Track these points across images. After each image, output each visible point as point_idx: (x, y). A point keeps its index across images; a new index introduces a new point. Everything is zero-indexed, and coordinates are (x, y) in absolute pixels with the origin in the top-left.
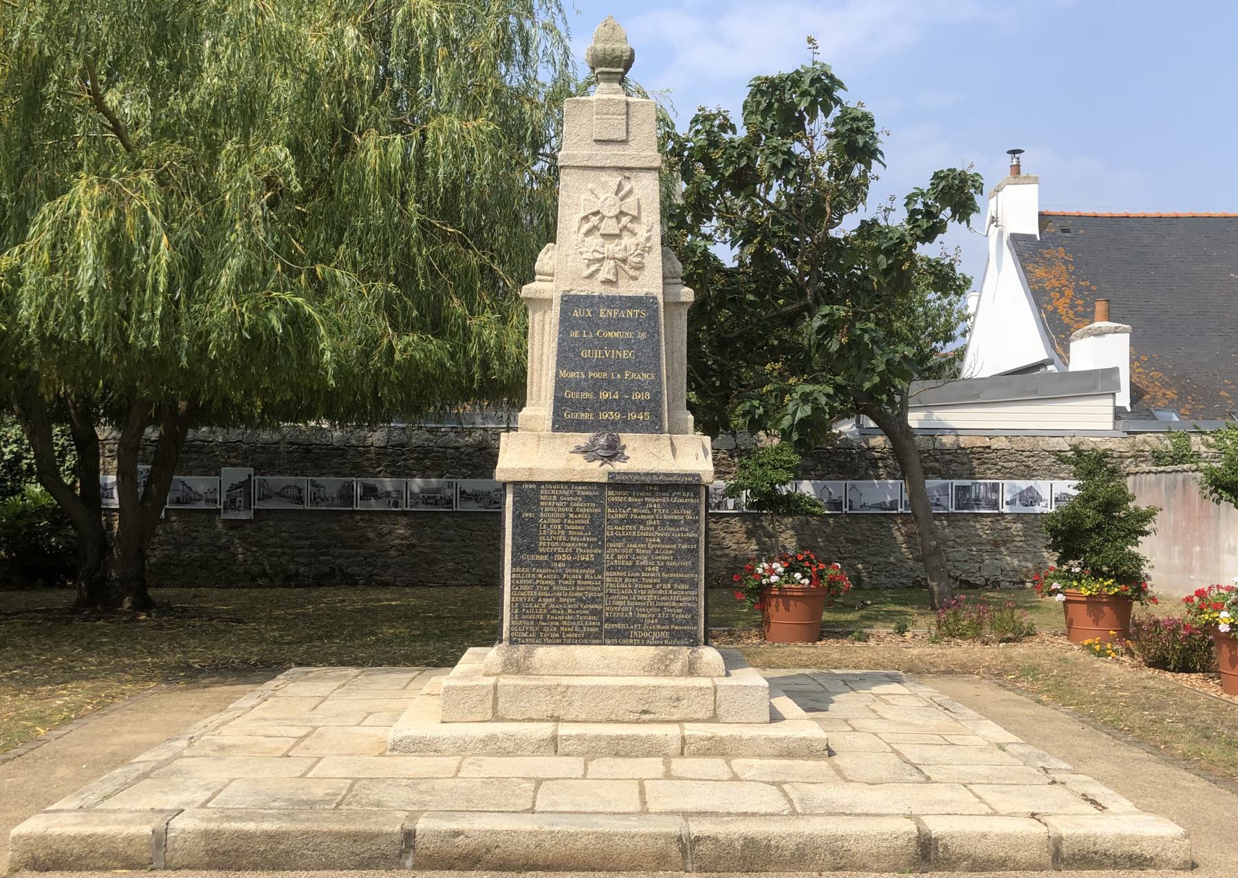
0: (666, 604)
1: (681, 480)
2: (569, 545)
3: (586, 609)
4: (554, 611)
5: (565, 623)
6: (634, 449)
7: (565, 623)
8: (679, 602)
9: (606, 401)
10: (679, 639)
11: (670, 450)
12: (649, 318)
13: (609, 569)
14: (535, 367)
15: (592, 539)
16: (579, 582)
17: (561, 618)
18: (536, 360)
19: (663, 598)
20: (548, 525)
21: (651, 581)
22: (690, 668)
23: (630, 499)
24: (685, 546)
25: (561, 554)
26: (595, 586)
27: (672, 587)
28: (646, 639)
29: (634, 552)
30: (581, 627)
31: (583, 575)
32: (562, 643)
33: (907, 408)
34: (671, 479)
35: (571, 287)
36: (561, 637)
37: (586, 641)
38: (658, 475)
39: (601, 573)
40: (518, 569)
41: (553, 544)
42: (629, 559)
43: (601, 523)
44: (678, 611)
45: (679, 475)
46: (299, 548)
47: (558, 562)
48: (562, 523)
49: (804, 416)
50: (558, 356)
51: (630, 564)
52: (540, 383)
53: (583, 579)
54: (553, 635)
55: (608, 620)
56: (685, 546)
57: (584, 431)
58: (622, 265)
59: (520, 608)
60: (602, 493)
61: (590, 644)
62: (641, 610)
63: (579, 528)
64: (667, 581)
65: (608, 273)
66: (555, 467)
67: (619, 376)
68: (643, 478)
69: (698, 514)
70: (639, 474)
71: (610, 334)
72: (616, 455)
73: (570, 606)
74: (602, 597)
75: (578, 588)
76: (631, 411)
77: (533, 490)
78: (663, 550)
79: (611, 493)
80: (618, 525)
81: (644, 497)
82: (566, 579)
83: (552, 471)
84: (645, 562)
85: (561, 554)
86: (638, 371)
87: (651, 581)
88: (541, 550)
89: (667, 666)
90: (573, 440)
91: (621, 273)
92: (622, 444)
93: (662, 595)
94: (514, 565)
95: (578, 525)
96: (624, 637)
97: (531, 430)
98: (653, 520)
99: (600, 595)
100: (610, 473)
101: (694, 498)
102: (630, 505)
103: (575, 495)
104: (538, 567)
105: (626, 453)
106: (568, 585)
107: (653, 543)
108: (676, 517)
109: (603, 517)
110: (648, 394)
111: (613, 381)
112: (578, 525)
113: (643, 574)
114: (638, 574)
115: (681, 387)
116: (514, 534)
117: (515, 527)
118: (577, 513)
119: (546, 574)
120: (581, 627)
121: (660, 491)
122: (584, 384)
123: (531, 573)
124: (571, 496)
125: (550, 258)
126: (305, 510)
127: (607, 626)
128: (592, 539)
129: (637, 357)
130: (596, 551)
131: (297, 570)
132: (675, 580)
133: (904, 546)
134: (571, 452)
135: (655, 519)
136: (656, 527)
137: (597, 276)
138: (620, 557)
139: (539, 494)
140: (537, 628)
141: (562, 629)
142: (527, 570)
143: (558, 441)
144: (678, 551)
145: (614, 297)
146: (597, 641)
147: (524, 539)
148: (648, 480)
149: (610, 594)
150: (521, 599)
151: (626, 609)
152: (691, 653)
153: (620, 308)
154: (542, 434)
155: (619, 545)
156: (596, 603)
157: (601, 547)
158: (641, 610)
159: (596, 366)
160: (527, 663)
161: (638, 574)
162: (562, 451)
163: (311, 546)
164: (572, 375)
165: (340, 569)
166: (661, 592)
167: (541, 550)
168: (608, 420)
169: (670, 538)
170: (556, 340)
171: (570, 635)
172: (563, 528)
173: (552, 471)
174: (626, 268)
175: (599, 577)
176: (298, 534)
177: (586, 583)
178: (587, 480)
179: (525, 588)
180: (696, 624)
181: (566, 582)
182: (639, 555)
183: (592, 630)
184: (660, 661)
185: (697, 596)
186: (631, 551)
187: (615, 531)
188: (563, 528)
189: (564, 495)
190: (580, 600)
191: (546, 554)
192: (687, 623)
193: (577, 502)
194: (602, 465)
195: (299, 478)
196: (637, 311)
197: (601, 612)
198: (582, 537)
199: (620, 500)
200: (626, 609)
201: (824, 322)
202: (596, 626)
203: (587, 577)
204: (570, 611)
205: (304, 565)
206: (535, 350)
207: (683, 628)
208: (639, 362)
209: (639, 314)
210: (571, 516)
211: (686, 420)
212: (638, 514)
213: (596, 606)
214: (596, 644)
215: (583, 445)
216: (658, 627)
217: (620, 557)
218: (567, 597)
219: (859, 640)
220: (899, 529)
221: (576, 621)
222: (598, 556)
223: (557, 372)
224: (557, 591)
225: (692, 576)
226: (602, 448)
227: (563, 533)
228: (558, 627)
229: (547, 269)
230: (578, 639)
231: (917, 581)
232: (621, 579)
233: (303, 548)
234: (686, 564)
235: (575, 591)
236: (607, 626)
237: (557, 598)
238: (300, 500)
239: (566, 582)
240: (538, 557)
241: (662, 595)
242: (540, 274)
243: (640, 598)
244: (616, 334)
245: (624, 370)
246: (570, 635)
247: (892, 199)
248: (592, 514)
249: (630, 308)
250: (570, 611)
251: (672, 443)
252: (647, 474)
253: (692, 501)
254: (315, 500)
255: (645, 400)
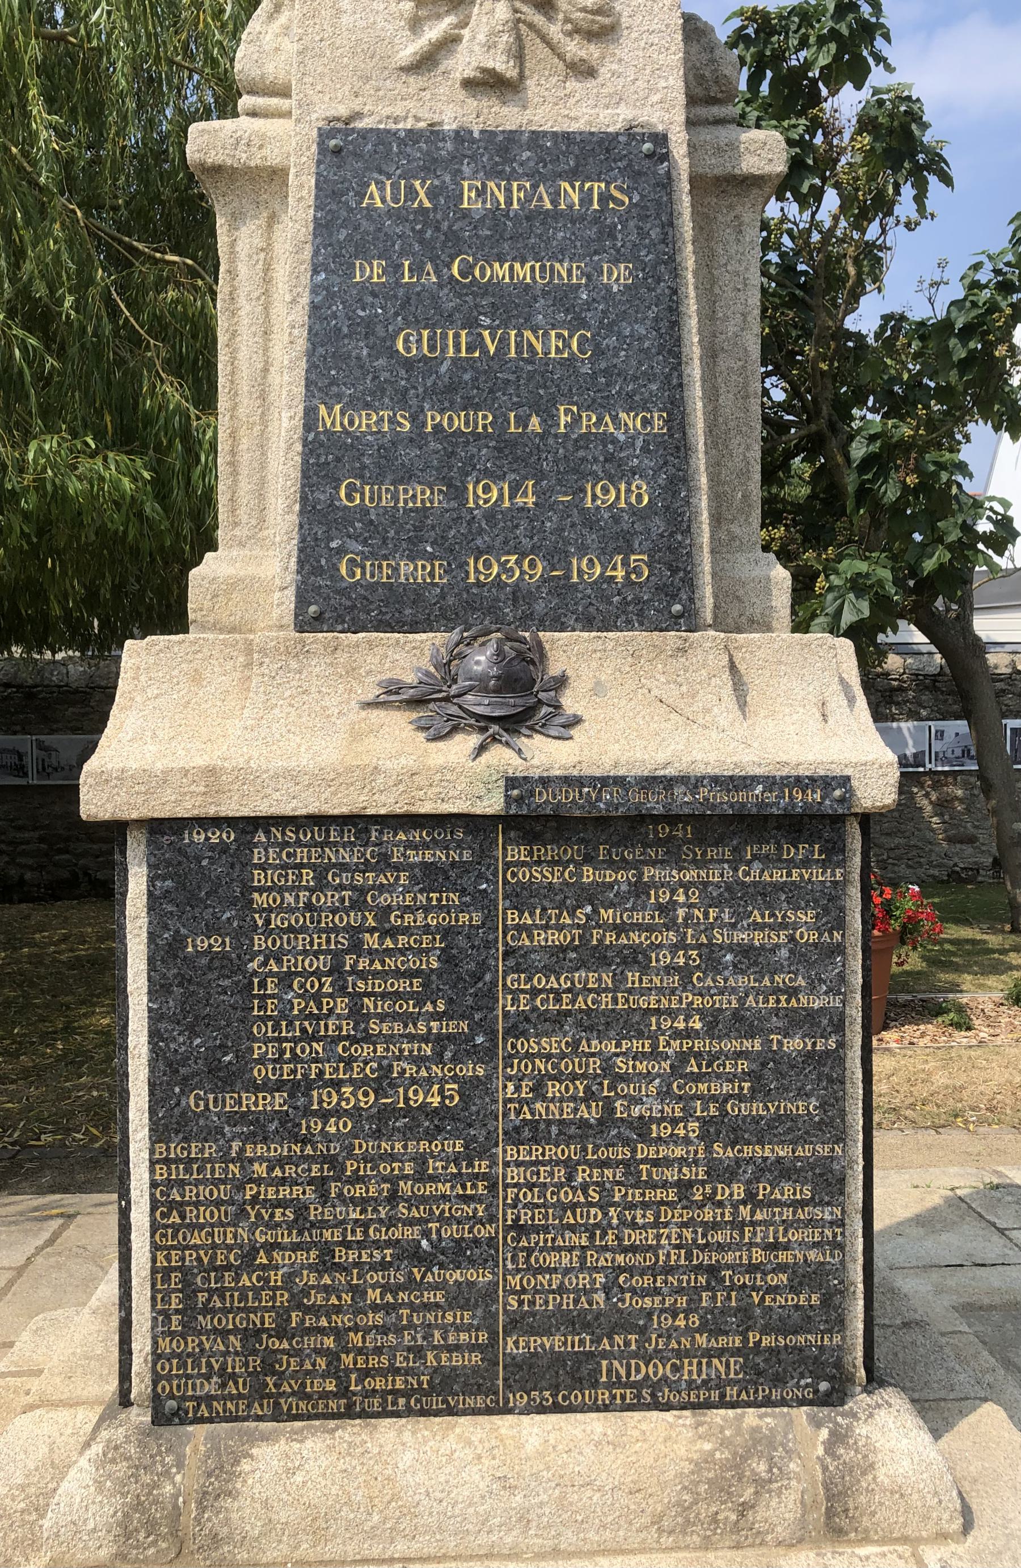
0: (730, 1257)
1: (778, 802)
2: (366, 1050)
3: (435, 1287)
4: (317, 1299)
5: (356, 1339)
6: (598, 689)
7: (356, 1339)
8: (775, 1246)
9: (491, 515)
10: (778, 1381)
11: (728, 690)
12: (640, 212)
13: (514, 1136)
14: (242, 411)
15: (450, 1027)
16: (405, 1188)
17: (342, 1320)
18: (244, 387)
19: (719, 1237)
20: (285, 980)
21: (671, 1175)
22: (830, 1514)
23: (589, 875)
24: (794, 1044)
25: (337, 1084)
26: (466, 1199)
27: (751, 1197)
28: (655, 1387)
29: (607, 1068)
30: (418, 1352)
31: (421, 1160)
32: (349, 1413)
33: (972, 609)
34: (741, 796)
35: (356, 105)
36: (344, 1391)
37: (436, 1402)
38: (692, 782)
39: (485, 1152)
40: (176, 1150)
41: (303, 1049)
42: (590, 1096)
43: (483, 966)
44: (773, 1280)
45: (770, 782)
46: (22, 843)
47: (325, 1116)
48: (336, 970)
49: (855, 619)
50: (310, 354)
51: (591, 1113)
52: (263, 466)
53: (421, 1176)
54: (315, 1386)
55: (516, 1324)
56: (794, 1044)
57: (414, 628)
58: (539, 19)
59: (189, 1291)
60: (484, 854)
61: (451, 1412)
62: (637, 1282)
63: (401, 985)
64: (728, 1173)
65: (490, 46)
66: (304, 760)
67: (535, 423)
68: (636, 797)
69: (840, 924)
70: (620, 781)
71: (501, 271)
72: (529, 712)
73: (377, 1277)
74: (492, 1241)
75: (402, 1209)
76: (583, 550)
77: (223, 848)
78: (713, 1057)
79: (517, 853)
80: (548, 971)
81: (637, 865)
82: (357, 1179)
83: (292, 776)
84: (651, 1107)
85: (337, 1084)
86: (602, 404)
87: (671, 1175)
88: (258, 1073)
89: (744, 1509)
90: (372, 660)
91: (536, 49)
92: (554, 669)
93: (715, 1226)
94: (159, 1133)
95: (398, 974)
96: (578, 1382)
97: (233, 630)
98: (674, 948)
99: (484, 1232)
100: (511, 782)
101: (824, 864)
102: (592, 895)
103: (384, 862)
104: (249, 1138)
105: (571, 702)
106: (363, 1203)
107: (677, 1034)
108: (758, 938)
109: (490, 944)
110: (641, 486)
111: (513, 443)
112: (398, 974)
113: (643, 1151)
114: (622, 1153)
115: (744, 474)
116: (155, 1017)
117: (157, 989)
118: (393, 932)
119: (281, 1162)
120: (418, 1352)
121: (700, 840)
122: (408, 454)
123: (226, 1159)
124: (366, 867)
125: (286, 30)
126: (29, 787)
127: (512, 1346)
128: (450, 1027)
129: (599, 352)
130: (468, 1070)
131: (22, 877)
132: (763, 1169)
133: (934, 820)
134: (368, 705)
135: (681, 945)
136: (685, 973)
137: (446, 64)
138: (553, 1089)
139: (247, 864)
140: (255, 1362)
141: (347, 1360)
142: (210, 1150)
143: (317, 666)
144: (769, 1058)
145: (512, 137)
146: (480, 1401)
147: (194, 1033)
148: (655, 803)
149: (519, 1228)
150: (190, 1257)
151: (583, 1280)
152: (830, 1448)
153: (537, 178)
154: (256, 638)
155: (551, 1044)
156: (472, 1262)
157: (487, 1055)
158: (637, 1282)
159: (451, 388)
160: (212, 1520)
161: (622, 1153)
162: (332, 702)
163: (41, 840)
164: (364, 421)
165: (86, 874)
166: (708, 1214)
167: (258, 1073)
168: (498, 583)
169: (737, 1016)
170: (305, 300)
171: (379, 1384)
172: (341, 990)
173: (295, 780)
174: (555, 30)
175: (481, 1166)
176: (20, 822)
177: (429, 1189)
178: (426, 808)
179: (205, 1215)
180: (840, 1323)
181: (359, 1191)
182: (625, 1078)
183: (457, 1360)
184: (721, 1488)
185: (842, 1224)
186: (595, 1065)
187: (535, 992)
188: (341, 990)
189: (343, 867)
190: (413, 1254)
191: (279, 1086)
192: (805, 1325)
193: (389, 888)
194: (481, 749)
195: (19, 737)
196: (598, 187)
197: (490, 1293)
198: (414, 1019)
199: (552, 876)
200: (583, 1280)
201: (875, 447)
202: (472, 1348)
203: (435, 1166)
204: (373, 1295)
205: (31, 868)
206: (243, 354)
207: (792, 1340)
208: (606, 372)
209: (605, 198)
210: (371, 941)
211: (766, 586)
212: (620, 929)
213: (472, 1275)
214: (475, 1412)
215: (410, 678)
216: (702, 1340)
217: (553, 1089)
218: (361, 1245)
219: (958, 1026)
220: (927, 795)
221: (399, 1331)
222: (469, 1087)
223: (310, 417)
224: (323, 1224)
225: (822, 1150)
226: (481, 685)
227: (341, 1006)
228: (333, 1357)
229: (273, 70)
230: (407, 1394)
231: (953, 872)
232: (560, 1173)
233: (28, 843)
234: (798, 1107)
235: (391, 1222)
236: (512, 1346)
237: (327, 1250)
238: (20, 770)
239: (359, 1191)
240: (248, 1100)
241: (715, 1226)
242: (251, 92)
243: (635, 1237)
244: (523, 271)
245: (554, 403)
246: (379, 1384)
247: (942, 265)
248: (447, 933)
249: (571, 176)
250: (373, 1295)
251: (733, 667)
252: (649, 782)
253: (817, 875)
254: (44, 771)
255: (632, 510)
